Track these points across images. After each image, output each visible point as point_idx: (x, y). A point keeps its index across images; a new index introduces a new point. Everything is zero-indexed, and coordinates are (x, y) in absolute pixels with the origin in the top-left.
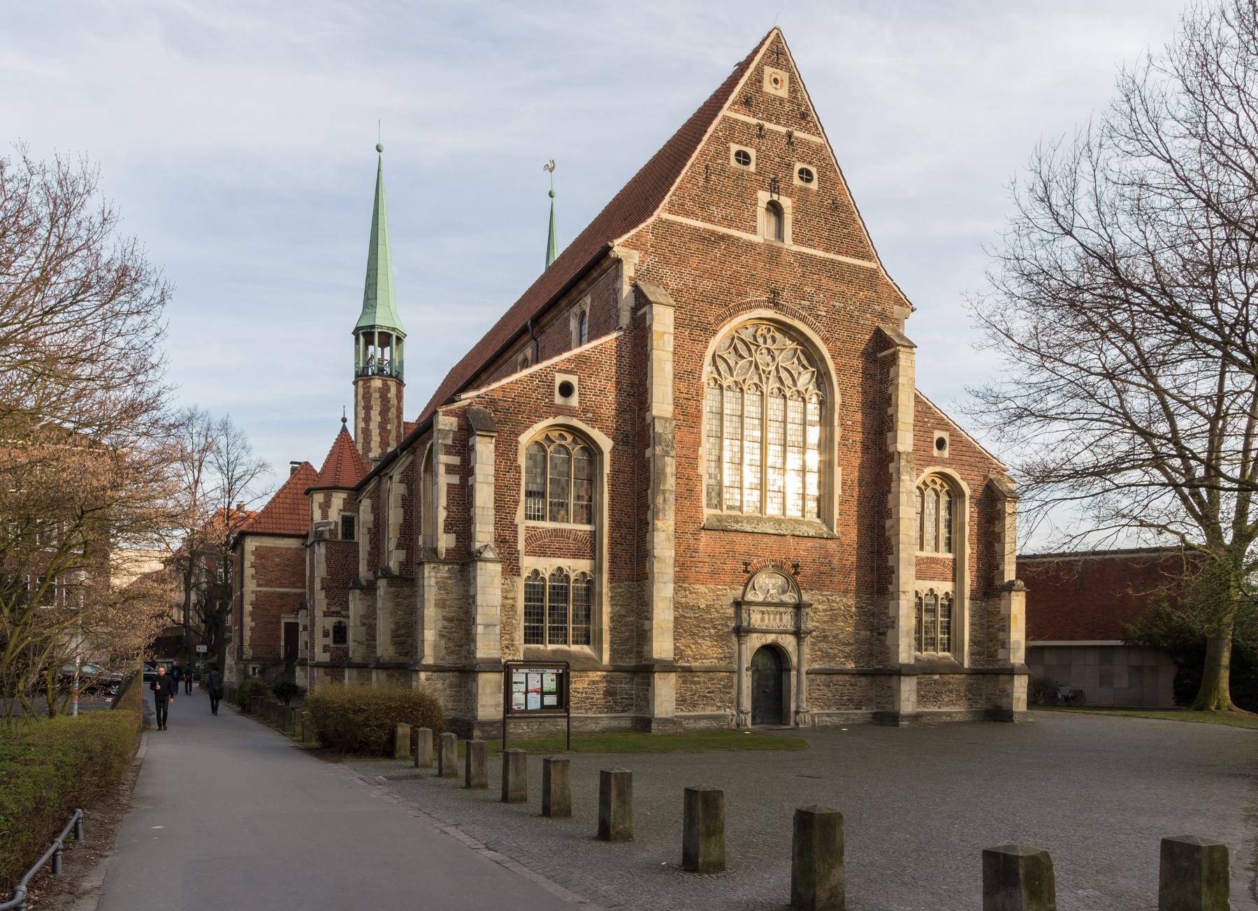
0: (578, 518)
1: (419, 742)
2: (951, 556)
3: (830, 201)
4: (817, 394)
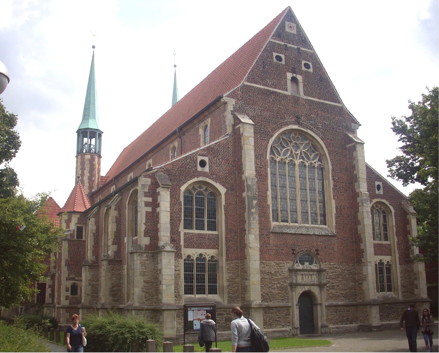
3: (319, 77)
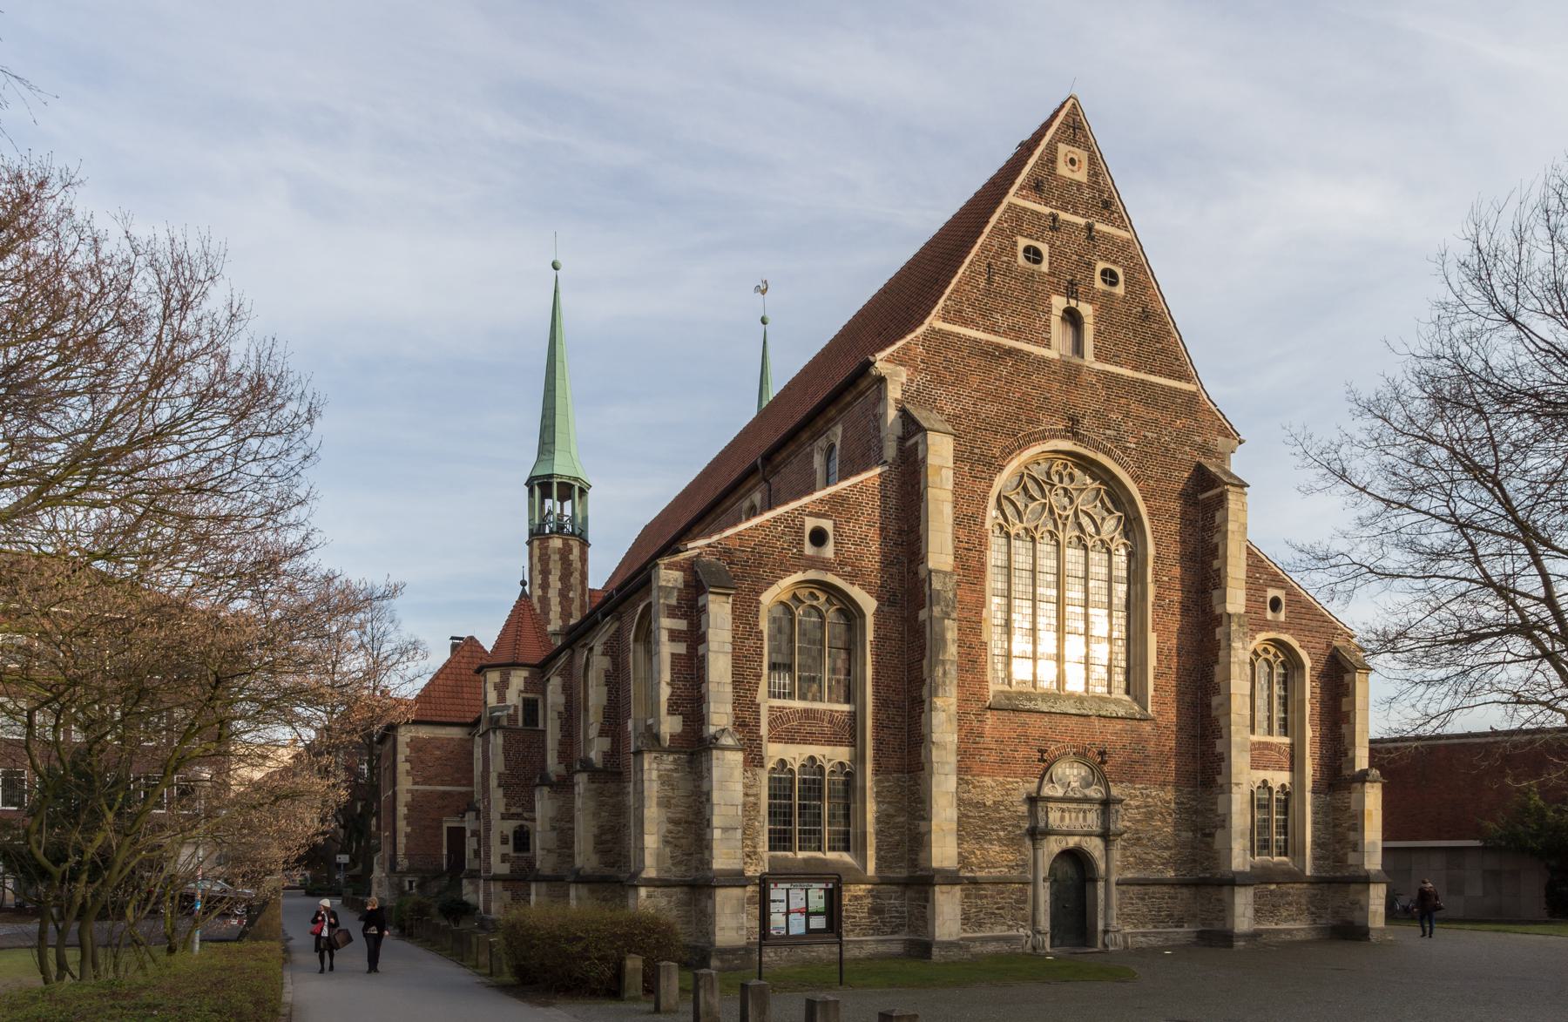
0: (834, 696)
1: (662, 980)
2: (1287, 740)
3: (1140, 309)
4: (1124, 544)
